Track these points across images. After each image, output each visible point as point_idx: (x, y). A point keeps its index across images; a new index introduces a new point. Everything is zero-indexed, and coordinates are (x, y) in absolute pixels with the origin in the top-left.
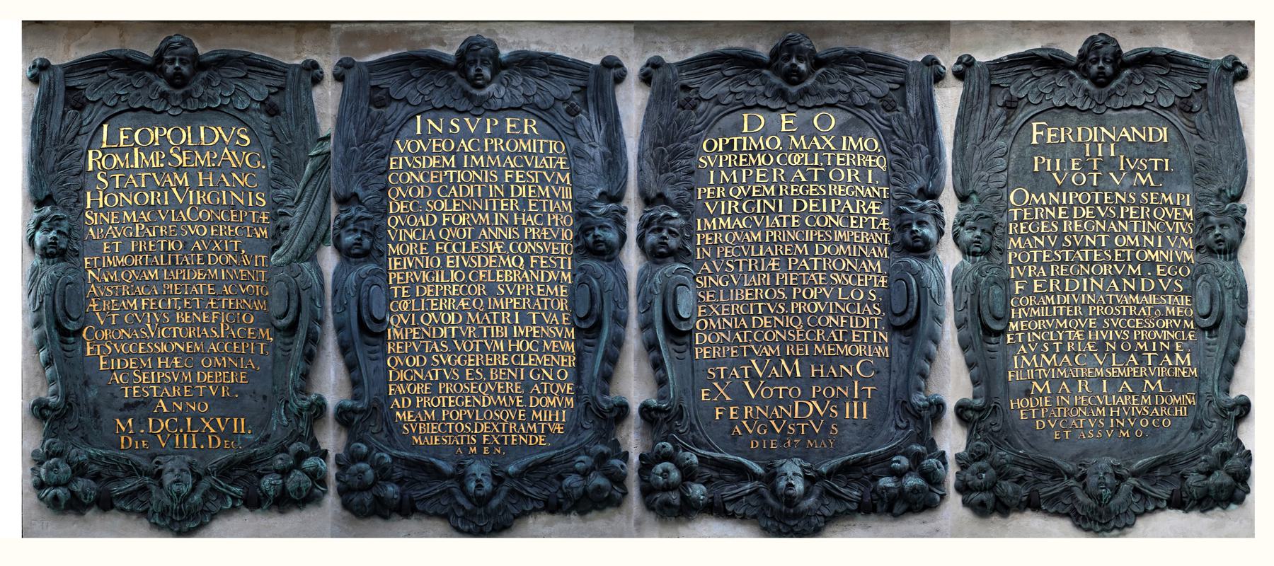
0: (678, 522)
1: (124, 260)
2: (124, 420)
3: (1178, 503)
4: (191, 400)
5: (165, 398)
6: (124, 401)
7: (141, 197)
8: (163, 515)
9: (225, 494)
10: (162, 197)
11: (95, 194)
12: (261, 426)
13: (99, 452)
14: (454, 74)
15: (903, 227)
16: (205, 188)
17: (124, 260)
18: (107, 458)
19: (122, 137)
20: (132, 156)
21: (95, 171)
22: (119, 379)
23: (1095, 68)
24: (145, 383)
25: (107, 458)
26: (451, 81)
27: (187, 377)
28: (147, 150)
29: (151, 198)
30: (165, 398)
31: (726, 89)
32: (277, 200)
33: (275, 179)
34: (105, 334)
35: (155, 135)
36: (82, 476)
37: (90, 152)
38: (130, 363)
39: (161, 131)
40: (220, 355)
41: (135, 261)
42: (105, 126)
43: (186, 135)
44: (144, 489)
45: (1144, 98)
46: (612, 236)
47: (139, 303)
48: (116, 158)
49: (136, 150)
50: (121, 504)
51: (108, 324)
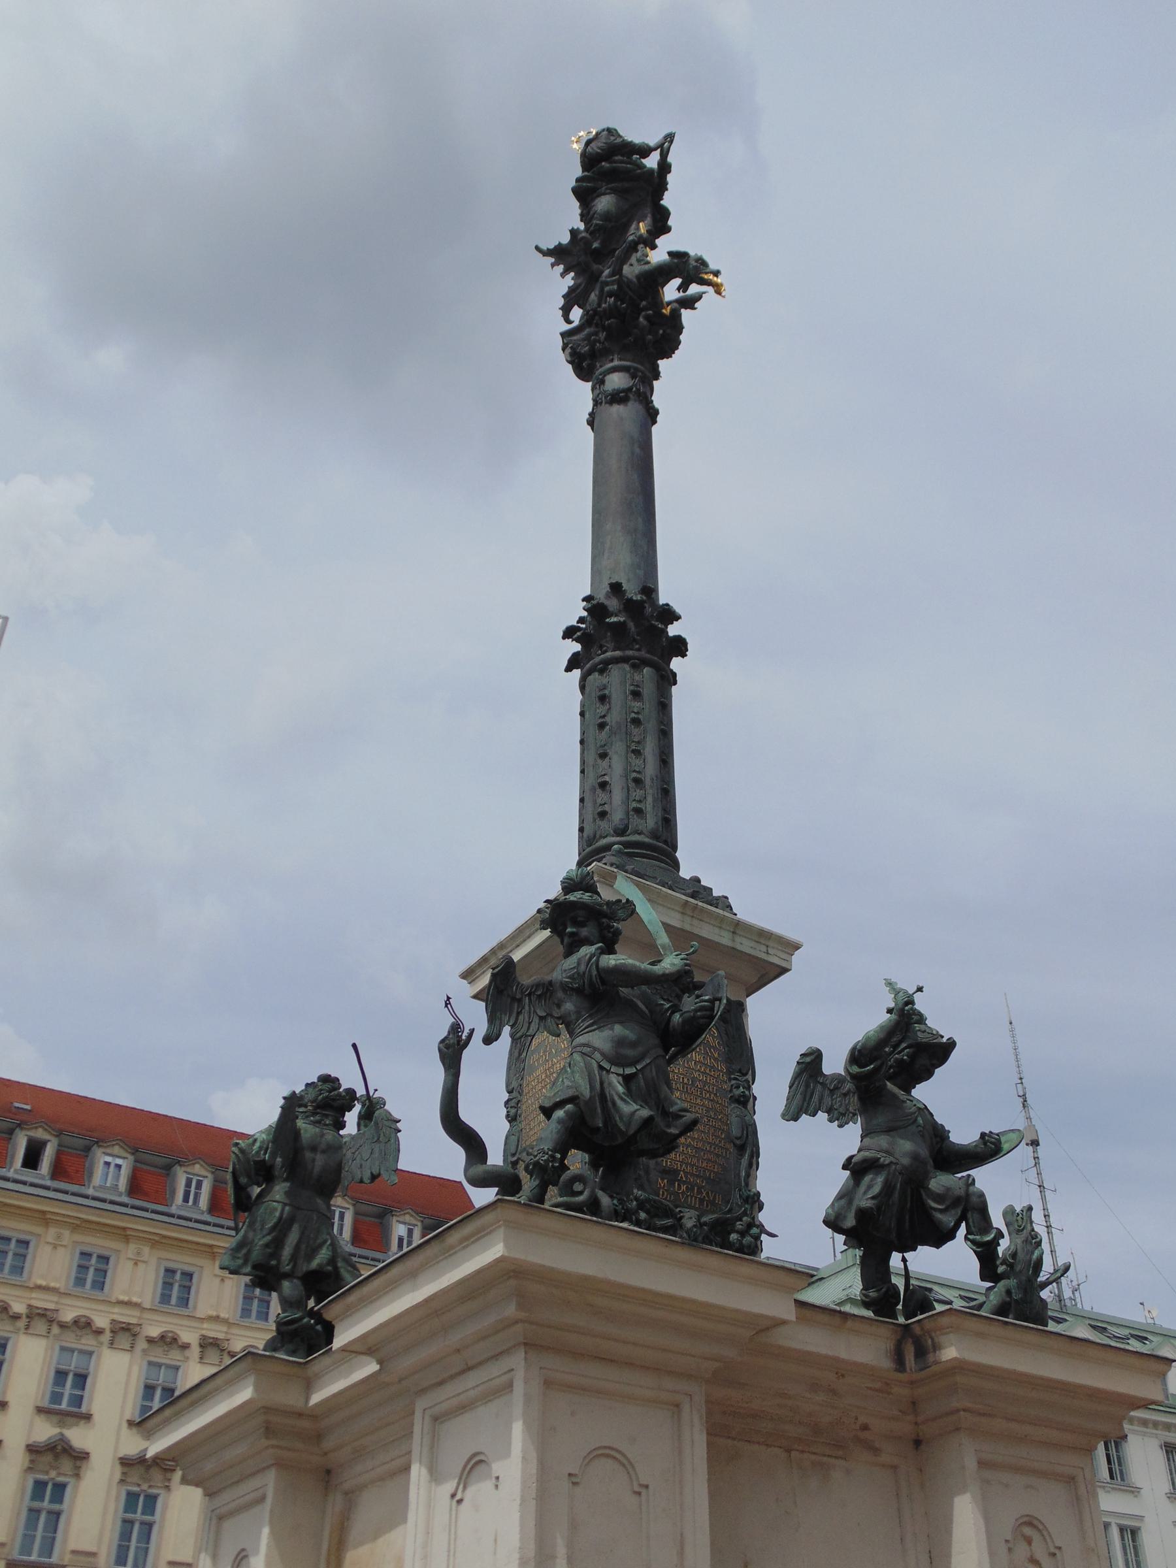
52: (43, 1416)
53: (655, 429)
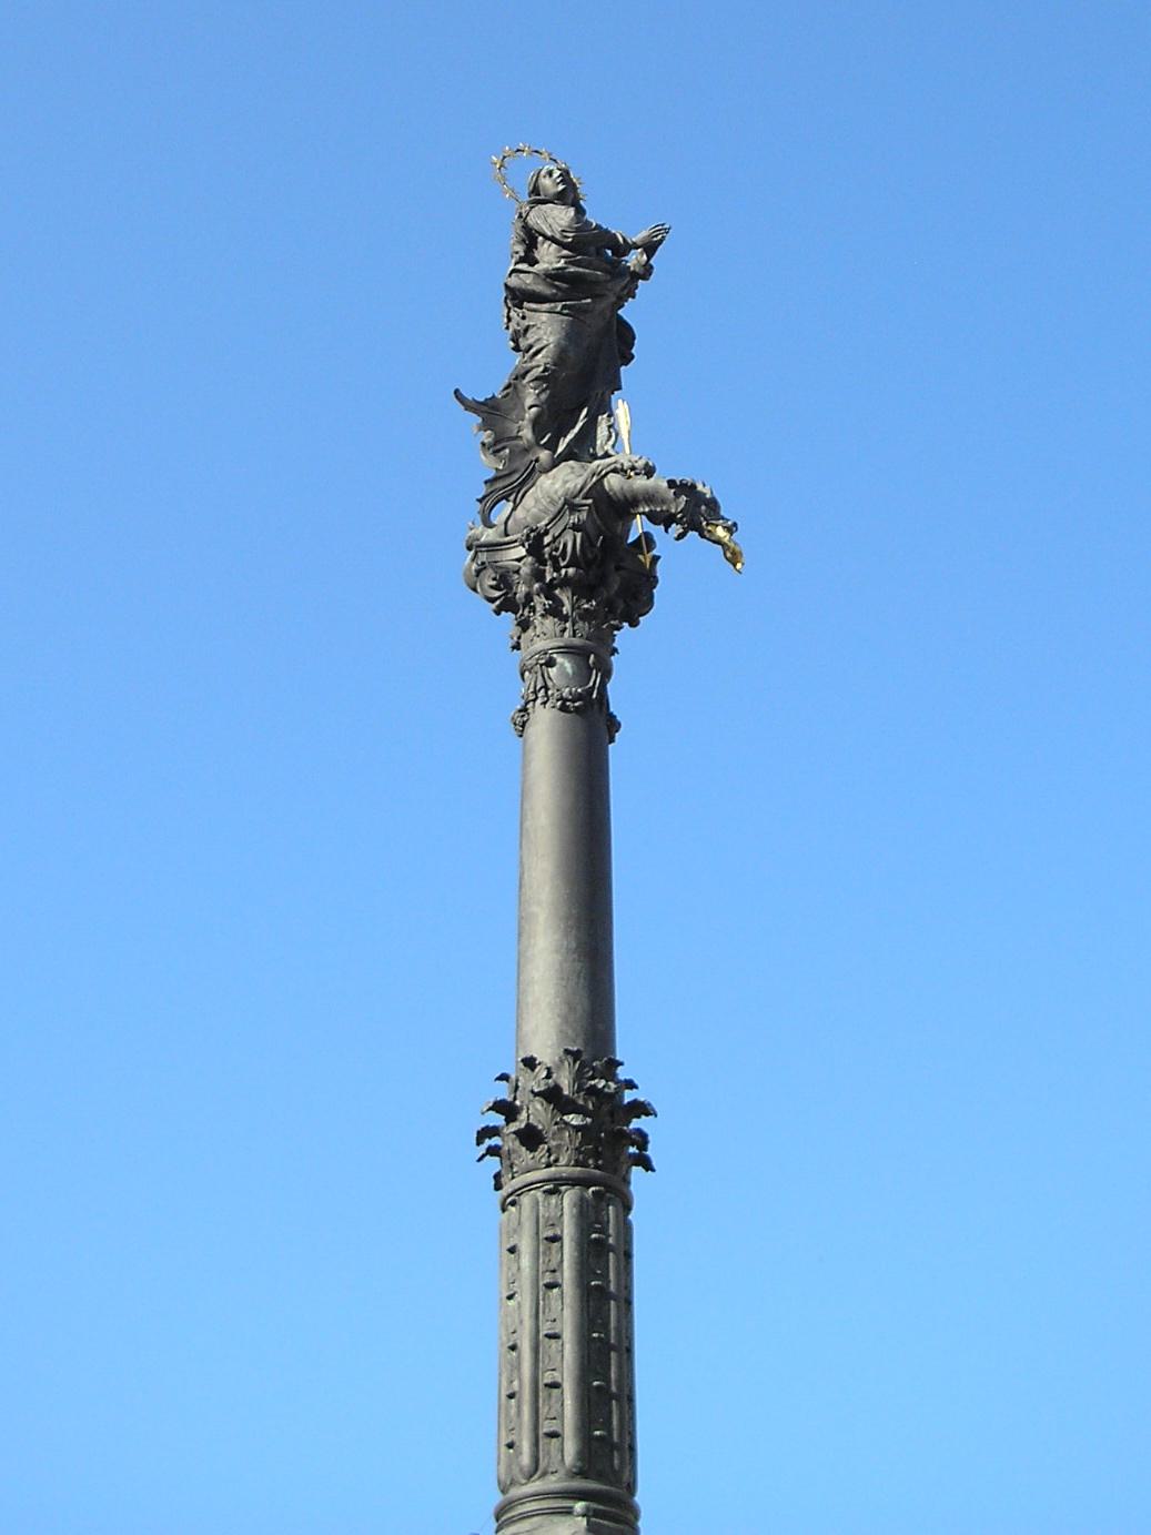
53: (618, 754)
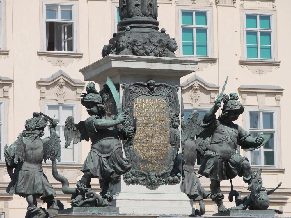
0: (118, 183)
1: (142, 128)
2: (142, 164)
3: (166, 183)
4: (155, 160)
5: (150, 159)
6: (142, 160)
7: (145, 114)
8: (149, 185)
9: (161, 181)
10: (149, 115)
11: (136, 113)
12: (168, 166)
13: (137, 171)
14: (146, 88)
15: (172, 122)
16: (157, 113)
17: (142, 128)
18: (139, 172)
19: (141, 101)
20: (143, 105)
21: (136, 108)
22: (141, 155)
23: (151, 87)
24: (146, 156)
25: (139, 172)
26: (146, 89)
27: (154, 155)
28: (146, 104)
29: (147, 115)
30: (150, 159)
31: (138, 91)
32: (171, 116)
33: (171, 111)
34: (138, 144)
35: (147, 101)
36: (134, 176)
37: (134, 103)
38: (143, 151)
39: (148, 100)
40: (161, 150)
41: (144, 129)
42: (137, 98)
43: (153, 101)
44: (146, 179)
45: (160, 94)
46: (177, 124)
47: (145, 138)
48: (140, 105)
49: (144, 104)
50: (141, 182)
51: (139, 143)
52: (245, 67)
